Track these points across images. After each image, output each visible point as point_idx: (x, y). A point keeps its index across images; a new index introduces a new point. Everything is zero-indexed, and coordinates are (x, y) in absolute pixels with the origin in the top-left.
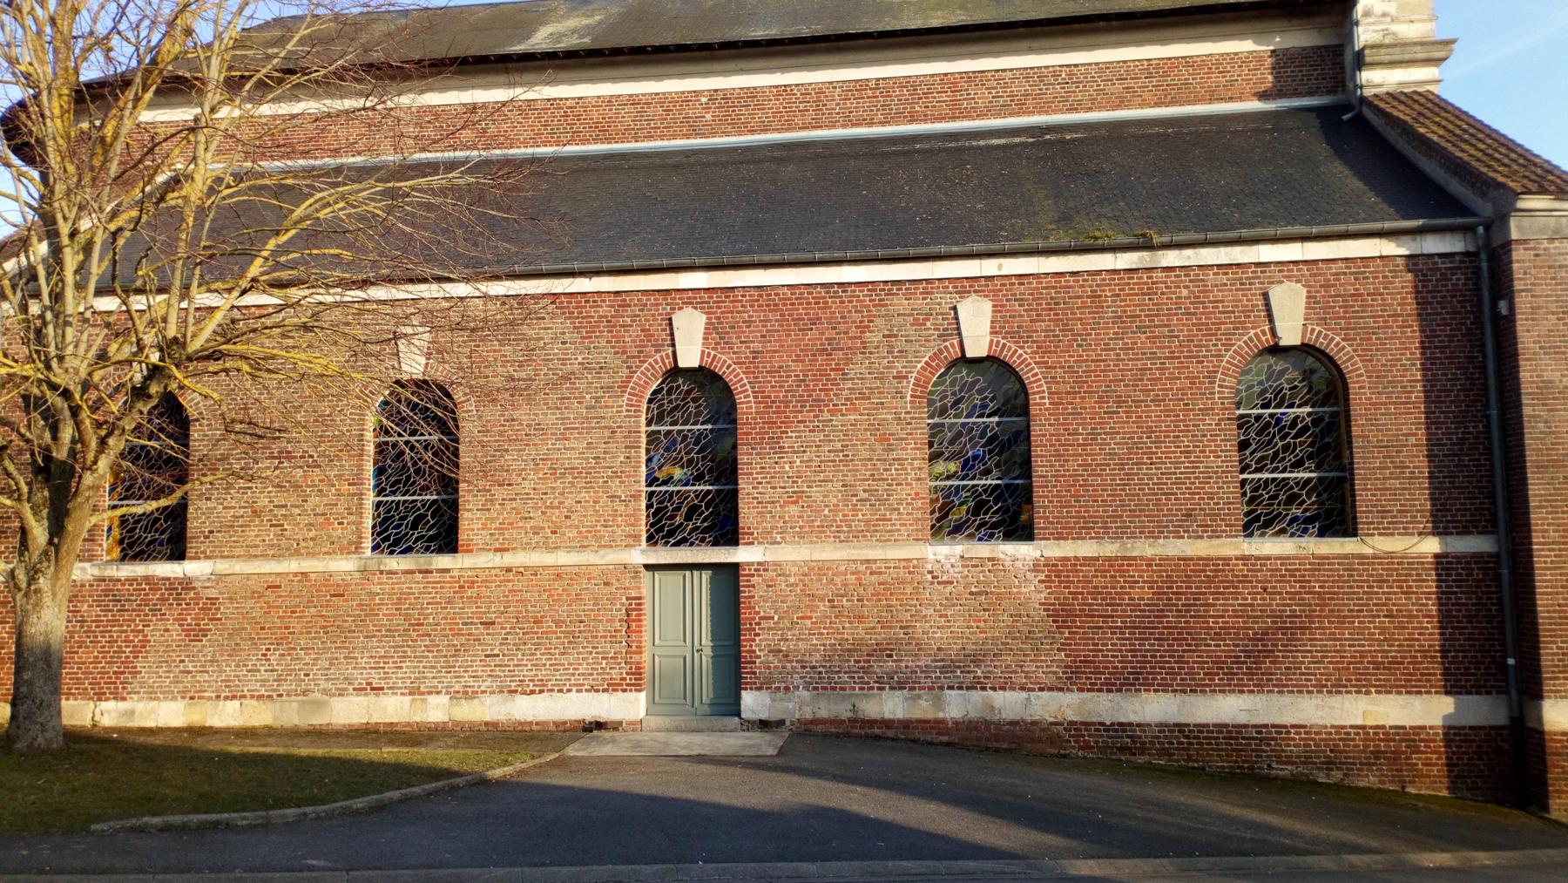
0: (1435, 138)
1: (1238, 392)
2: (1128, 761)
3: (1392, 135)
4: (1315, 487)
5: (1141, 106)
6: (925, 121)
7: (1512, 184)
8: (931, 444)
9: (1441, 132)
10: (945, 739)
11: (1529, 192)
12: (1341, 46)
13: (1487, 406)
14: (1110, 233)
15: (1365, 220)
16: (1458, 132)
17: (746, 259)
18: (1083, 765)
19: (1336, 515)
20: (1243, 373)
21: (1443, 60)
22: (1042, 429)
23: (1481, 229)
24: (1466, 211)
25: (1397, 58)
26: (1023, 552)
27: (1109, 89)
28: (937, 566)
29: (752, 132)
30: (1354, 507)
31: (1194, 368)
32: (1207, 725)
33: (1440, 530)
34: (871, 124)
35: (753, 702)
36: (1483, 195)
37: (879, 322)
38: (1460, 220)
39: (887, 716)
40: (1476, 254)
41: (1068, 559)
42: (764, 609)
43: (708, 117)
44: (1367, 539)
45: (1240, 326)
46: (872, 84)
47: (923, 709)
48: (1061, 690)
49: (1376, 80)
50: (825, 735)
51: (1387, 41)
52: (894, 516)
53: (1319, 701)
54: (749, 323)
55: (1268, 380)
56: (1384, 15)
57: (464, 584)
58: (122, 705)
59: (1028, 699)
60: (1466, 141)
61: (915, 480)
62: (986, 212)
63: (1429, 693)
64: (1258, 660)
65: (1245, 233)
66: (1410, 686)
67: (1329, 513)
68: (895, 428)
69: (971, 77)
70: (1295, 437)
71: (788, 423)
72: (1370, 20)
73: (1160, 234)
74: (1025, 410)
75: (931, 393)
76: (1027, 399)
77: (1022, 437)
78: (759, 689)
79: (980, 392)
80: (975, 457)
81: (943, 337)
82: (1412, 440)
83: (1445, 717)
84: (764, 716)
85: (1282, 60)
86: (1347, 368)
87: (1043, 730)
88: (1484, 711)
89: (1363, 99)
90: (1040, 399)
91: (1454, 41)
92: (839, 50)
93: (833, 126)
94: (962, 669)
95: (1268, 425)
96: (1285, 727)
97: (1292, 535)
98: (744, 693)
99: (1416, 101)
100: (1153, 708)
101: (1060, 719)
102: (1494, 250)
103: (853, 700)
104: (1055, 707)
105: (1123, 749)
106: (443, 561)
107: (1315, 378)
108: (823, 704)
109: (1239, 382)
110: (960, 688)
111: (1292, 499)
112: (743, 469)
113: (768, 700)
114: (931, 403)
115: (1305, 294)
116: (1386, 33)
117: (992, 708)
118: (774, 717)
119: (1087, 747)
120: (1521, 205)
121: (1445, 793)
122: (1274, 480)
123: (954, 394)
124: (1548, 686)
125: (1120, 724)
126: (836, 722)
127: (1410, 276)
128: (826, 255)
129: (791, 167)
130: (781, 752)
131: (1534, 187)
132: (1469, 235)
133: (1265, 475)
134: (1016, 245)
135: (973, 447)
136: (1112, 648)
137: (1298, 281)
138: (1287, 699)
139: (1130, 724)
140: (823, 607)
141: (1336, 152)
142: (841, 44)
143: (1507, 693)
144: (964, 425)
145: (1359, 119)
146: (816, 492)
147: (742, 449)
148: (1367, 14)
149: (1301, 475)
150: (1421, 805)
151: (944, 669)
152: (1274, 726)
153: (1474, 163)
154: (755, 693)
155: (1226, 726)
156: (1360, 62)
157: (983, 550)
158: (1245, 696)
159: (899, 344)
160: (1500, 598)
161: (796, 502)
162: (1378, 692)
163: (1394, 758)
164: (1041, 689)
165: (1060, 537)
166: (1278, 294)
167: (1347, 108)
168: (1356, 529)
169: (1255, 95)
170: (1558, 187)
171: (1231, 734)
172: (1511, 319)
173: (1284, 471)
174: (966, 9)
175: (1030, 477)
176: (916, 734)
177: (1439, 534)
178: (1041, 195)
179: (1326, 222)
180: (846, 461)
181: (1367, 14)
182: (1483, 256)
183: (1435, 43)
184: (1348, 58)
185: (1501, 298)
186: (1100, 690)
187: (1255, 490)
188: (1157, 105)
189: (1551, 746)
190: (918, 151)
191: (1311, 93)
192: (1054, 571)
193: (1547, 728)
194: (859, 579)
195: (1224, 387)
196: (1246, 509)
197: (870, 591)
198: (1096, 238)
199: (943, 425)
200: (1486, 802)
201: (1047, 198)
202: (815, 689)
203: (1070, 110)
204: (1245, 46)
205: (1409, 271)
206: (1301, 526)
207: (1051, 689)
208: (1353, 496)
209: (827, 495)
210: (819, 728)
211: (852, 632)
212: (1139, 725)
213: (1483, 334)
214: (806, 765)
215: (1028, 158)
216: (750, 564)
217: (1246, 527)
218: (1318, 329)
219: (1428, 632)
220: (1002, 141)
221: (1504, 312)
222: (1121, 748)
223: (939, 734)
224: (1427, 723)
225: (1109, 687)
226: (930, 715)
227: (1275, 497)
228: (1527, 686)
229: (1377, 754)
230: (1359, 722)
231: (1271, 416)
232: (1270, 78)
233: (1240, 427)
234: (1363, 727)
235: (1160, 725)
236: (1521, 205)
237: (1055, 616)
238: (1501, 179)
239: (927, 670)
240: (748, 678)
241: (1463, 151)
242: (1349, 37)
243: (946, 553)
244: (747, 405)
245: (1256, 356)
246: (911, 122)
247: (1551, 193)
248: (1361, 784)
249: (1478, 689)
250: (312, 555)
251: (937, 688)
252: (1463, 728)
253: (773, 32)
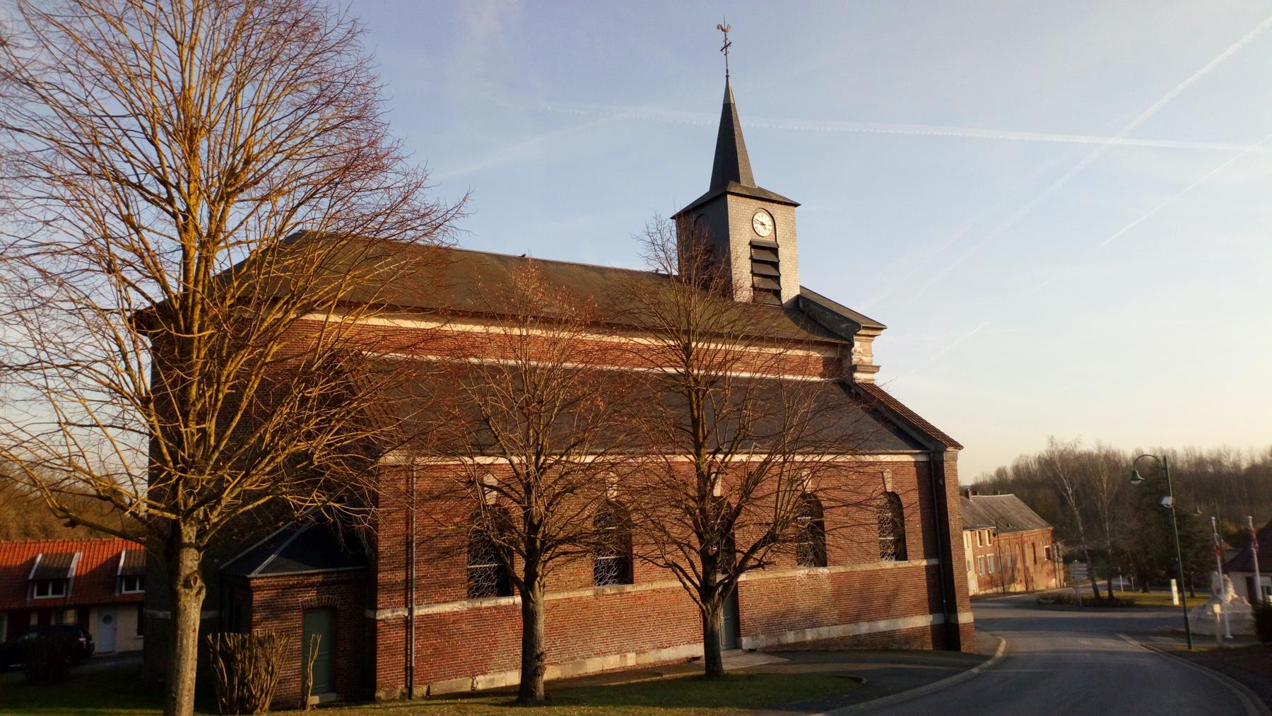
19: (901, 555)
26: (823, 571)
35: (746, 642)
49: (860, 377)
57: (640, 597)
58: (488, 677)
94: (812, 620)
100: (864, 628)
106: (628, 588)
156: (854, 368)
192: (831, 576)
211: (776, 607)
219: (923, 592)
225: (850, 622)
250: (573, 589)
251: (802, 629)
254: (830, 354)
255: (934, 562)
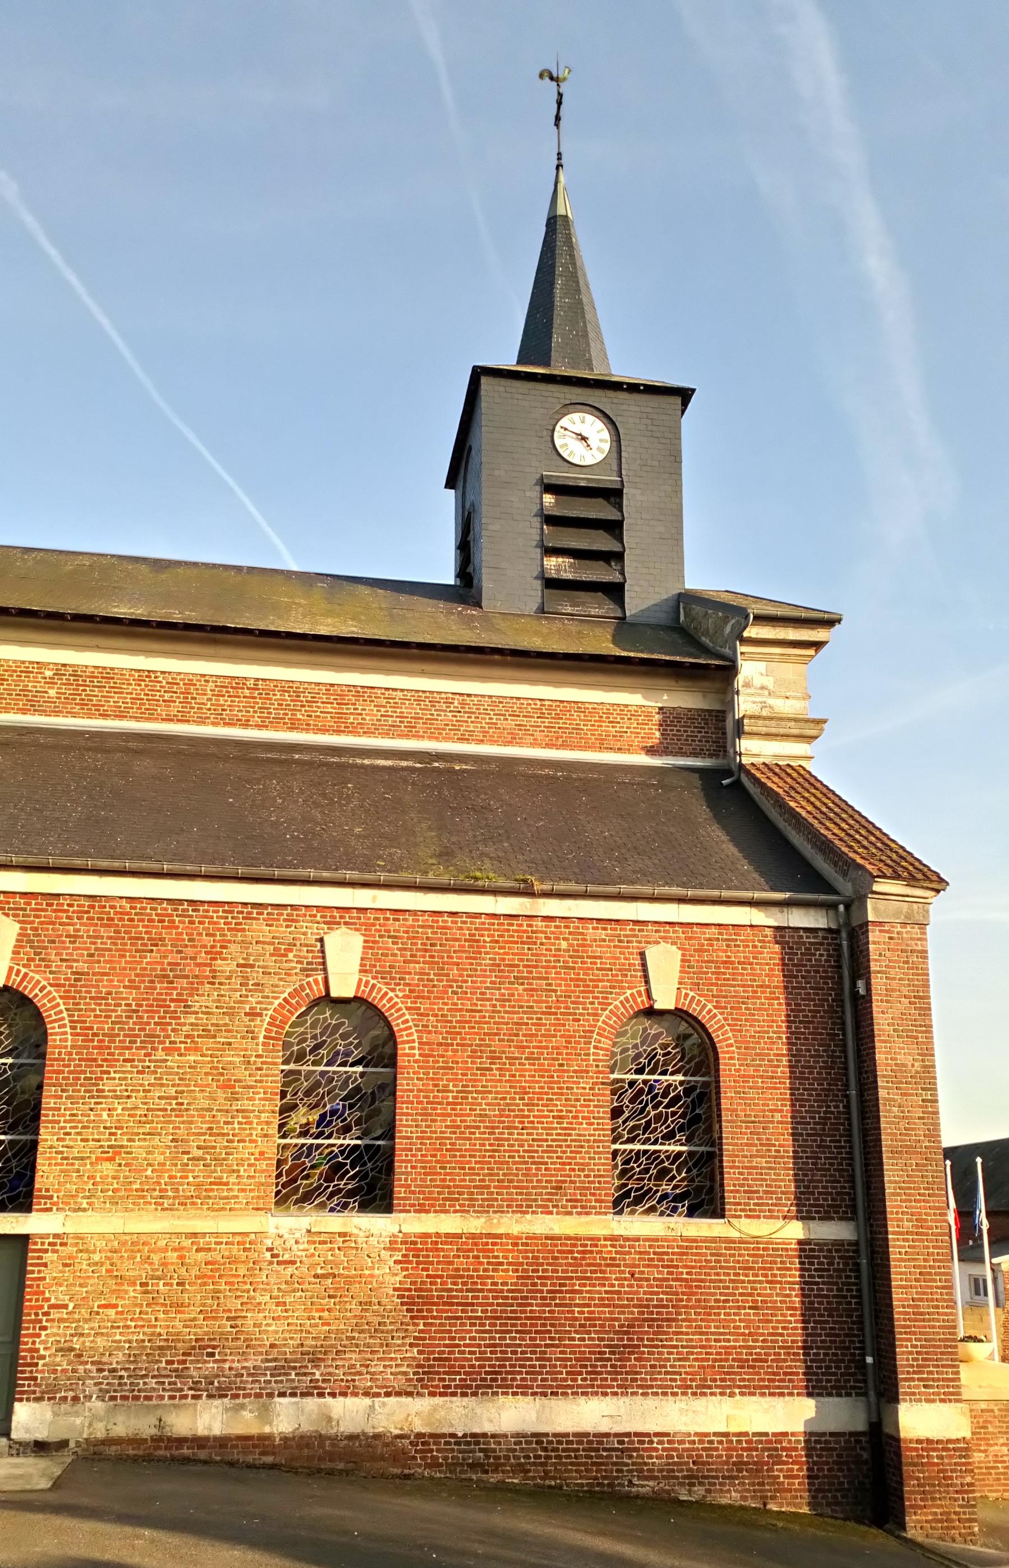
0: (804, 814)
1: (613, 1054)
2: (479, 1481)
3: (766, 805)
4: (685, 1162)
5: (534, 744)
6: (307, 730)
7: (869, 867)
8: (283, 1094)
9: (810, 808)
10: (269, 1459)
11: (885, 877)
12: (724, 712)
13: (847, 1085)
14: (491, 875)
15: (737, 888)
16: (824, 809)
17: (78, 862)
18: (428, 1488)
19: (704, 1198)
20: (619, 1035)
21: (816, 737)
22: (409, 1082)
23: (841, 908)
24: (829, 888)
25: (773, 731)
27: (501, 723)
28: (278, 1242)
29: (105, 716)
30: (722, 1185)
31: (571, 1026)
32: (567, 1435)
33: (804, 1215)
34: (246, 725)
36: (845, 874)
37: (233, 948)
38: (823, 897)
39: (201, 1431)
40: (837, 932)
41: (427, 1235)
42: (56, 1295)
43: (52, 693)
44: (733, 1221)
45: (616, 985)
46: (250, 683)
47: (246, 1422)
48: (409, 1394)
49: (754, 750)
50: (120, 1459)
51: (765, 713)
52: (233, 1180)
53: (683, 1405)
54: (74, 938)
55: (643, 1043)
56: (763, 688)
59: (372, 1407)
60: (831, 819)
61: (259, 1142)
62: (365, 837)
63: (791, 1394)
64: (620, 1361)
65: (624, 888)
66: (773, 1387)
67: (699, 1190)
68: (242, 1073)
69: (361, 691)
70: (667, 1107)
71: (111, 1062)
72: (749, 691)
73: (542, 880)
74: (391, 1061)
75: (288, 1034)
76: (395, 1048)
77: (388, 1089)
78: (38, 1400)
79: (344, 1037)
80: (333, 1112)
81: (306, 971)
82: (778, 1117)
83: (807, 1422)
84: (41, 1435)
85: (669, 718)
86: (717, 1036)
87: (387, 1445)
88: (845, 1415)
89: (741, 766)
90: (409, 1049)
91: (825, 721)
92: (215, 642)
93: (202, 721)
94: (300, 1371)
95: (641, 1091)
96: (648, 1435)
97: (662, 1214)
98: (17, 1405)
99: (789, 775)
100: (510, 1415)
101: (406, 1431)
102: (853, 929)
103: (159, 1413)
104: (403, 1416)
105: (474, 1466)
107: (688, 1043)
108: (120, 1418)
109: (614, 1044)
110: (293, 1395)
111: (662, 1173)
112: (47, 1115)
113: (49, 1415)
114: (286, 1045)
115: (679, 957)
116: (764, 705)
117: (330, 1419)
118: (54, 1438)
119: (435, 1465)
120: (876, 887)
121: (805, 1510)
122: (645, 1152)
123: (315, 1037)
124: (903, 1388)
125: (474, 1435)
126: (136, 1441)
127: (777, 948)
128: (177, 867)
129: (147, 762)
130: (57, 1484)
131: (888, 872)
132: (831, 913)
133: (637, 1147)
134: (393, 877)
135: (331, 1101)
136: (470, 1342)
137: (673, 943)
138: (651, 1402)
139: (484, 1435)
140: (133, 1292)
141: (715, 816)
142: (218, 636)
143: (865, 1394)
144: (323, 1073)
145: (738, 784)
146: (138, 1149)
147: (48, 1091)
148: (747, 685)
149: (671, 1148)
150: (780, 1524)
151: (276, 1371)
152: (636, 1434)
153: (837, 842)
154: (33, 1405)
155: (586, 1435)
156: (739, 730)
157: (333, 1222)
158: (608, 1398)
159: (255, 975)
160: (859, 1290)
161: (111, 1159)
162: (742, 1394)
163: (757, 1469)
164: (388, 1394)
165: (422, 1210)
166: (653, 954)
167: (728, 773)
168: (723, 1210)
169: (643, 748)
170: (910, 874)
171: (592, 1444)
172: (868, 998)
173: (655, 1143)
174: (360, 621)
175: (393, 1138)
176: (236, 1455)
177: (802, 1218)
178: (423, 825)
179: (701, 886)
180: (180, 1110)
181: (747, 685)
182: (844, 935)
183: (807, 721)
184: (729, 725)
185: (860, 977)
186: (454, 1394)
187: (626, 1162)
188: (549, 746)
189: (908, 1456)
190: (297, 762)
191: (695, 754)
192: (414, 1250)
193: (903, 1435)
194: (182, 1257)
195: (599, 1049)
196: (617, 1182)
197: (195, 1272)
198: (476, 879)
199: (299, 1072)
200: (845, 1519)
201: (430, 829)
202: (113, 1398)
203: (461, 740)
204: (634, 699)
205: (777, 943)
206: (670, 1204)
207: (399, 1394)
208: (722, 1173)
209: (151, 1151)
210: (113, 1451)
211: (167, 1324)
212: (493, 1436)
213: (843, 1012)
214: (85, 1501)
215: (413, 784)
216: (42, 1236)
217: (616, 1203)
218: (691, 994)
219: (790, 1326)
220: (389, 763)
221: (862, 991)
222: (473, 1466)
223: (262, 1454)
224: (789, 1429)
225: (465, 1390)
226: (254, 1430)
227: (646, 1171)
228: (883, 1389)
229: (740, 1465)
230: (723, 1429)
231: (645, 1082)
232: (658, 734)
233: (613, 1092)
234: (726, 1435)
235: (517, 1435)
236: (876, 887)
237: (409, 1303)
238: (859, 861)
239: (255, 1373)
240: (25, 1385)
241: (827, 829)
242: (731, 704)
243: (292, 1226)
244: (60, 1036)
245: (631, 1018)
246: (291, 729)
247: (904, 879)
248: (724, 1501)
249: (838, 1390)
252: (824, 1434)
253: (139, 612)
254: (684, 699)
255: (835, 1231)
